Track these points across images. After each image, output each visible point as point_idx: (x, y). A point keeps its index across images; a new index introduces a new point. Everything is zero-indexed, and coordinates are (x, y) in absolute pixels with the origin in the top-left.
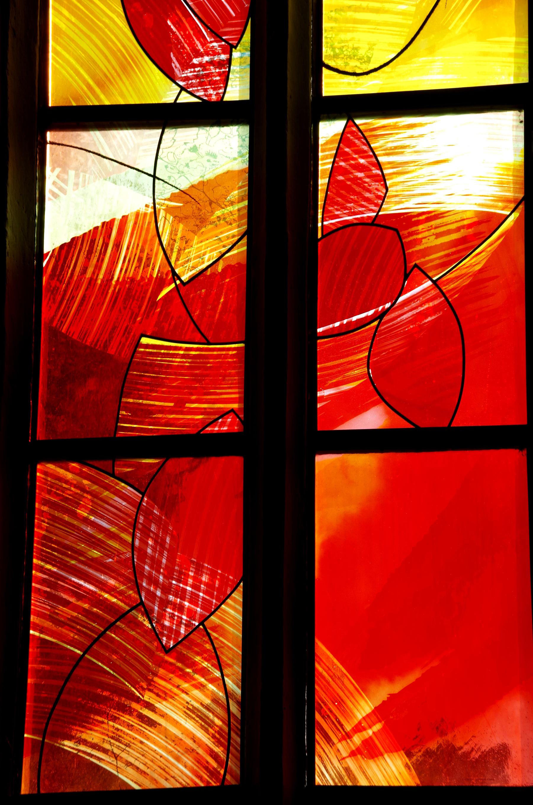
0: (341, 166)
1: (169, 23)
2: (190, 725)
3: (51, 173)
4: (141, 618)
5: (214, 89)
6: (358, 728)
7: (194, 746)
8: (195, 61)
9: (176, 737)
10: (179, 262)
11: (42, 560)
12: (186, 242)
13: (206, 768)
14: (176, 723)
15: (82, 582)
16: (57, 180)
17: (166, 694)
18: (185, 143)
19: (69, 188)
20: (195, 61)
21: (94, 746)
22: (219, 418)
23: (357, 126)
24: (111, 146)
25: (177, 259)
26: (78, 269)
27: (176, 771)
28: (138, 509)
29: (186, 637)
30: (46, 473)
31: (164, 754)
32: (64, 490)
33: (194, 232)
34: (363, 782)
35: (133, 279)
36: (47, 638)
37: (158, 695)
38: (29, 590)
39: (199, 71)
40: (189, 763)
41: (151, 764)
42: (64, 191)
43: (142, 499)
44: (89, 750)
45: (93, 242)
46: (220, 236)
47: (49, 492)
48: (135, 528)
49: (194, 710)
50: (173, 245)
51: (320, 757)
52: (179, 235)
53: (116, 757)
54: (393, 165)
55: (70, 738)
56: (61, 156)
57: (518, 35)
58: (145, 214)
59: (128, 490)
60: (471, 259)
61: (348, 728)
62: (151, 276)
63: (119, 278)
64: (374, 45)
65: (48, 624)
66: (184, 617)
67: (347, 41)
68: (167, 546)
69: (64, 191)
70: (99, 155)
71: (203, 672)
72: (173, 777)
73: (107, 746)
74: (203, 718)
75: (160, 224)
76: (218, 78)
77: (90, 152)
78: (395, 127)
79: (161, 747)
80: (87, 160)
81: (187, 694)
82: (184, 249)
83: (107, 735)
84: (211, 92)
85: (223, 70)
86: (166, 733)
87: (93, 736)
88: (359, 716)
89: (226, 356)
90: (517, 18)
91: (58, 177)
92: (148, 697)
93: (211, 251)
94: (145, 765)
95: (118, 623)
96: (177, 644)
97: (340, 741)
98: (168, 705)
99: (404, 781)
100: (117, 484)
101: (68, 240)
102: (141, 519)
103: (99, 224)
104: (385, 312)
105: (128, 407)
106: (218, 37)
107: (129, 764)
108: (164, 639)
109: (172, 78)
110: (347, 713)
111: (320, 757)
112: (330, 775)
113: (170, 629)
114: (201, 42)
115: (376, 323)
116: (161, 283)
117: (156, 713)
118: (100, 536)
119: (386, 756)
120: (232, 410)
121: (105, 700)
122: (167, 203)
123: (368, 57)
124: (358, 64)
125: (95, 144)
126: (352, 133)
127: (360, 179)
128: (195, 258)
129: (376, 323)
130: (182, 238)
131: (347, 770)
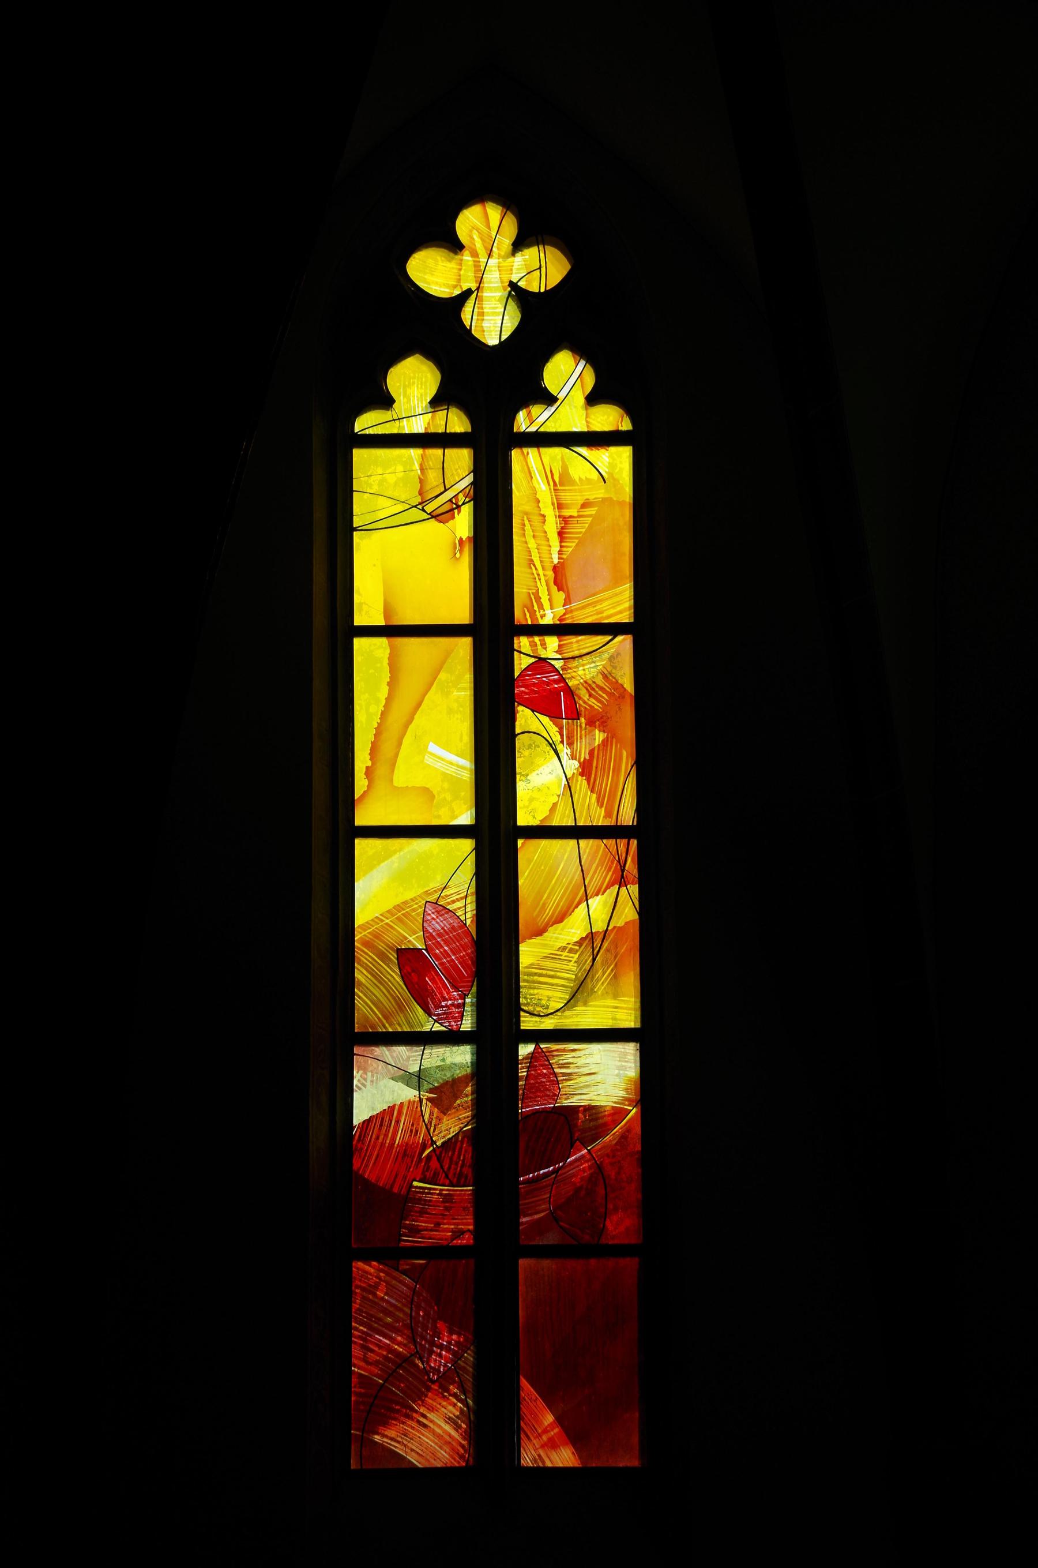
0: (532, 1074)
1: (427, 979)
2: (447, 1427)
3: (357, 1074)
4: (417, 1361)
5: (455, 1022)
6: (545, 1431)
7: (450, 1440)
8: (443, 1004)
9: (440, 1434)
10: (435, 1133)
11: (358, 1324)
12: (439, 1120)
13: (458, 1454)
14: (439, 1426)
15: (381, 1338)
16: (361, 1079)
17: (433, 1408)
18: (438, 1056)
19: (368, 1084)
20: (443, 1004)
21: (392, 1439)
22: (460, 1235)
23: (541, 1049)
24: (392, 1057)
25: (434, 1131)
26: (374, 1137)
27: (440, 1455)
28: (414, 1292)
29: (444, 1374)
30: (358, 1269)
31: (433, 1444)
32: (369, 1279)
33: (445, 1114)
34: (549, 1464)
35: (407, 1144)
36: (363, 1372)
37: (428, 1409)
38: (350, 1342)
39: (445, 1010)
40: (447, 1450)
41: (425, 1450)
42: (365, 1086)
43: (416, 1286)
44: (389, 1441)
45: (383, 1119)
46: (460, 1117)
47: (360, 1281)
48: (412, 1304)
49: (450, 1418)
50: (431, 1122)
51: (523, 1448)
52: (435, 1115)
53: (405, 1446)
54: (564, 1074)
55: (378, 1434)
56: (363, 1063)
57: (635, 997)
58: (414, 1101)
59: (407, 1280)
60: (610, 1137)
61: (540, 1431)
62: (418, 1142)
63: (399, 1143)
64: (551, 998)
65: (362, 1364)
66: (443, 1361)
67: (534, 995)
68: (431, 1316)
69: (365, 1086)
70: (386, 1063)
71: (455, 1395)
72: (439, 1458)
73: (399, 1439)
74: (455, 1423)
75: (423, 1108)
76: (457, 1015)
77: (380, 1060)
78: (564, 1050)
79: (431, 1440)
80: (378, 1066)
81: (445, 1408)
82: (438, 1124)
83: (399, 1433)
84: (453, 1023)
85: (460, 1010)
86: (434, 1432)
87: (392, 1433)
88: (546, 1424)
89: (464, 1195)
90: (635, 987)
91: (361, 1076)
92: (422, 1410)
93: (455, 1126)
94: (422, 1451)
95: (403, 1364)
96: (439, 1378)
97: (535, 1438)
98: (435, 1415)
99: (573, 1464)
100: (401, 1276)
101: (367, 1118)
102: (416, 1299)
103: (386, 1108)
104: (560, 1168)
105: (406, 1227)
106: (456, 989)
107: (412, 1450)
108: (431, 1374)
109: (430, 1014)
110: (539, 1422)
111: (523, 1448)
112: (529, 1458)
113: (434, 1368)
114: (446, 992)
115: (595, 952)
116: (424, 1147)
117: (427, 1419)
118: (391, 1309)
119: (561, 1448)
120: (469, 1230)
121: (398, 1412)
122: (427, 1094)
123: (547, 1005)
124: (542, 1010)
125: (383, 1056)
126: (538, 1053)
127: (544, 1082)
128: (445, 1131)
129: (554, 1176)
130: (436, 1118)
131: (539, 1456)
